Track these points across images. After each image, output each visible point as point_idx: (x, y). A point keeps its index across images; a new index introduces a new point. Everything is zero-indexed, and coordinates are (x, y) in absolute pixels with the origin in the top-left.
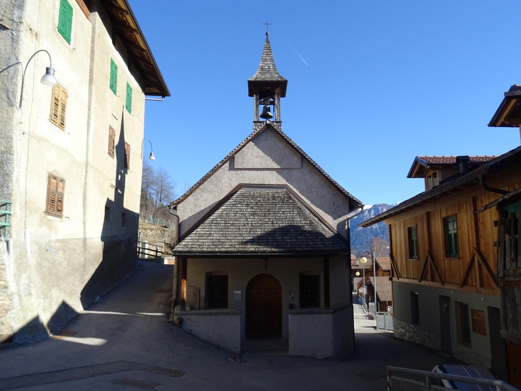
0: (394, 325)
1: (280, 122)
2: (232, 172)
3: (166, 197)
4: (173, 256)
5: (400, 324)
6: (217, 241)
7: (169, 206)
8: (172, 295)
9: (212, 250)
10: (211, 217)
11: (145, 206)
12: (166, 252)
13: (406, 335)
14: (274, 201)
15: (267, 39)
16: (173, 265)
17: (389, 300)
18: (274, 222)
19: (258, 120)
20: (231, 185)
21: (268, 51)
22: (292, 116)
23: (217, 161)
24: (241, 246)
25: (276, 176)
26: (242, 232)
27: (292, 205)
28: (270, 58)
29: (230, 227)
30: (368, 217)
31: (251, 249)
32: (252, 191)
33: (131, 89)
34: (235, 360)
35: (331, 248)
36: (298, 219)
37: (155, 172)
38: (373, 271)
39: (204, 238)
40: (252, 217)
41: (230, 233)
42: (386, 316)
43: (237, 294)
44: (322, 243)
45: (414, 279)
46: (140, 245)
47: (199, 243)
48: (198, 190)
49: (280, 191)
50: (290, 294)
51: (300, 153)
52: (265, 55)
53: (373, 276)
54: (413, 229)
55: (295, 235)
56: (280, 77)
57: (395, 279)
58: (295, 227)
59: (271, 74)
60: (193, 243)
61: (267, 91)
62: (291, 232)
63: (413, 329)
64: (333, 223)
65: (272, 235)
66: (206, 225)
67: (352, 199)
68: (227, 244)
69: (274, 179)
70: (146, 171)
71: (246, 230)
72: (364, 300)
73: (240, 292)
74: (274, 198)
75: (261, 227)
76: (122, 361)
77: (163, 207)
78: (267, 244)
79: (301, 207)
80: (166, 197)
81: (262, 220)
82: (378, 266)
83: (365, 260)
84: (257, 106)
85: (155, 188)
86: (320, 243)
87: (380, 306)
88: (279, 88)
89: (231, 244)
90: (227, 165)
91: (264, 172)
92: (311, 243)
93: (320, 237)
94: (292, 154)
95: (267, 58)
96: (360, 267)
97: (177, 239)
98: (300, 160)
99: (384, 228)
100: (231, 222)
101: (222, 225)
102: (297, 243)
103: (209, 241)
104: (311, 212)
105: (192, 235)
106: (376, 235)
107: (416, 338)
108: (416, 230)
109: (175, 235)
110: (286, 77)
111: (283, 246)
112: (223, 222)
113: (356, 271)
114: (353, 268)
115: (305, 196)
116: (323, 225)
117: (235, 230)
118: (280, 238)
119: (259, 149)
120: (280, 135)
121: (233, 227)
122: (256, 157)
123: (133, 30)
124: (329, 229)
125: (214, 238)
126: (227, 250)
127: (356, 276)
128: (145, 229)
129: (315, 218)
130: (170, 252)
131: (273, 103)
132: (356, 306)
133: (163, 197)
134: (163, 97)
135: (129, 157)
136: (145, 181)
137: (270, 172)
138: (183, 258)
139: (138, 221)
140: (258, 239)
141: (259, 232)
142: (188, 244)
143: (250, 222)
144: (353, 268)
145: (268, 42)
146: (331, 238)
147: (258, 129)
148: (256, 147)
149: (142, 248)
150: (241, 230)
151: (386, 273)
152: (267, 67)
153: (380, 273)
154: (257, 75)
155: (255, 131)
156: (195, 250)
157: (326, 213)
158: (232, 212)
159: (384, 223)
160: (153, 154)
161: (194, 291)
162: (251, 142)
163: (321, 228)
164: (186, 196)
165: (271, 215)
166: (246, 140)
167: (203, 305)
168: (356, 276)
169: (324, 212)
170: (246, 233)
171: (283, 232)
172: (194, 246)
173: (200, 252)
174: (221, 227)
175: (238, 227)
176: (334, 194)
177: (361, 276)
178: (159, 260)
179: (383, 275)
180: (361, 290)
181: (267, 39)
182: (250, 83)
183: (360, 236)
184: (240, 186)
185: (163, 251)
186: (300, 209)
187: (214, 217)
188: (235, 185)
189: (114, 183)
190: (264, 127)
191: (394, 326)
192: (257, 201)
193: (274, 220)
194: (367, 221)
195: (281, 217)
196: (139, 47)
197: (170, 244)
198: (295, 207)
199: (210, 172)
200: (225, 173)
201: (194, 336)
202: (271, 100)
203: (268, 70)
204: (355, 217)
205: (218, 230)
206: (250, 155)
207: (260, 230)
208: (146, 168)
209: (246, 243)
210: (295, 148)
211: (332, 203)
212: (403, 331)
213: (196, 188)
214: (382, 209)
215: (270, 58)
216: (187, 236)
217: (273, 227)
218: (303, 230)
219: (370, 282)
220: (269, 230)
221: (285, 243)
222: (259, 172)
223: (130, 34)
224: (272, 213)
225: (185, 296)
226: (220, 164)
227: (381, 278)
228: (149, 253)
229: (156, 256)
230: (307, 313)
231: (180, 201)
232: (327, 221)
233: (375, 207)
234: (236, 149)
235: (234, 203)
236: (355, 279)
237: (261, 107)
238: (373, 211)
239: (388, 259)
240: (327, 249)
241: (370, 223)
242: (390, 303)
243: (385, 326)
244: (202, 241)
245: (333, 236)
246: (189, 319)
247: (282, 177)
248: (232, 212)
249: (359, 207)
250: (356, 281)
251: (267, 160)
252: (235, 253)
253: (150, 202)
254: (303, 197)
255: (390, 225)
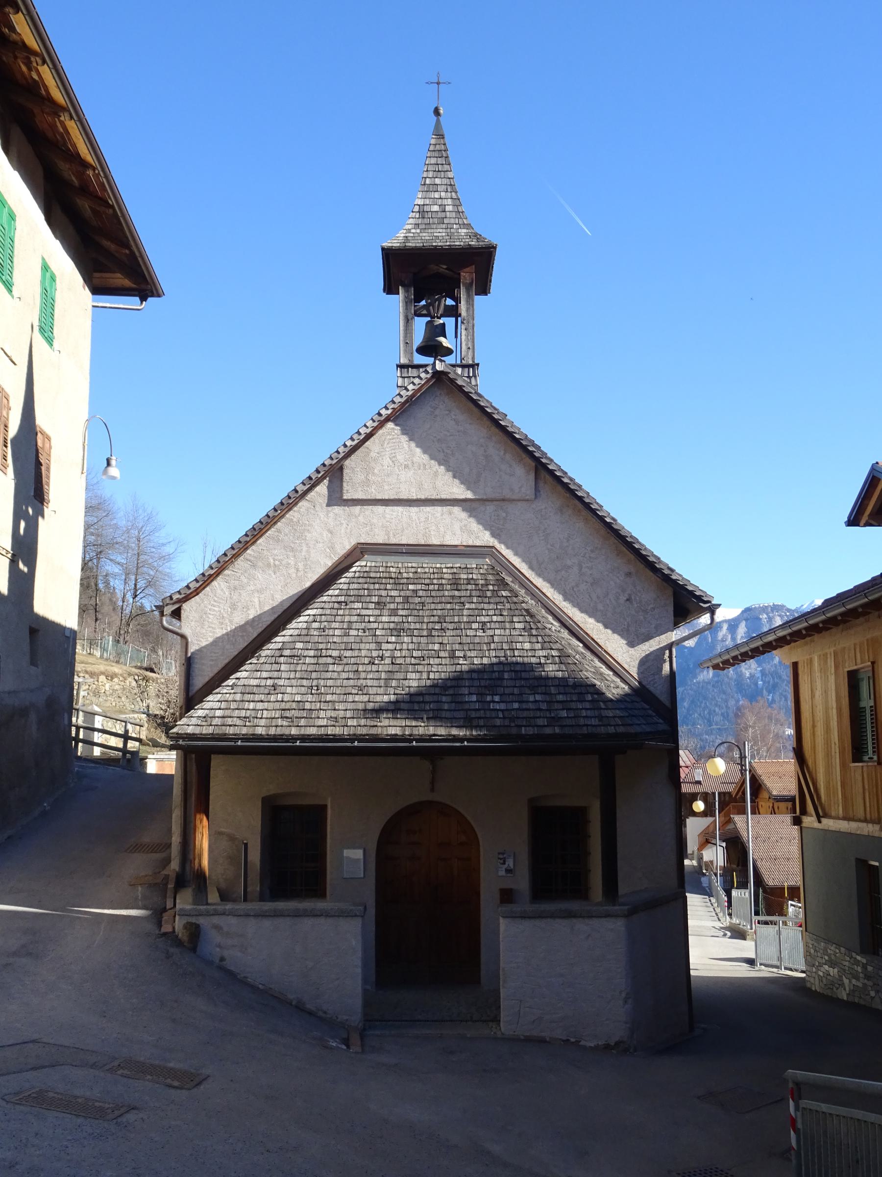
0: (807, 955)
1: (474, 366)
2: (337, 509)
3: (149, 584)
4: (171, 748)
5: (825, 952)
6: (294, 705)
7: (161, 609)
8: (167, 861)
9: (279, 731)
10: (278, 639)
11: (92, 612)
12: (152, 740)
13: (842, 985)
14: (457, 593)
15: (438, 125)
16: (172, 775)
17: (792, 883)
18: (458, 654)
19: (411, 360)
20: (332, 548)
21: (440, 161)
22: (503, 345)
23: (295, 479)
24: (363, 722)
25: (461, 521)
26: (364, 682)
27: (508, 606)
28: (445, 181)
29: (331, 668)
30: (729, 643)
31: (392, 731)
32: (395, 564)
33: (53, 279)
34: (348, 1046)
35: (621, 730)
36: (527, 646)
37: (121, 514)
38: (744, 800)
39: (257, 698)
40: (393, 639)
41: (330, 683)
42: (785, 932)
43: (350, 858)
44: (596, 713)
45: (865, 821)
46: (79, 719)
47: (243, 713)
48: (240, 562)
49: (473, 563)
50: (503, 859)
51: (531, 454)
52: (431, 174)
53: (743, 811)
54: (864, 676)
55: (516, 691)
56: (476, 235)
57: (809, 821)
58: (518, 668)
59: (449, 227)
60: (228, 713)
61: (436, 276)
62: (505, 683)
63: (864, 967)
64: (628, 656)
65: (451, 692)
66: (262, 660)
67: (683, 587)
68: (322, 714)
69: (458, 529)
70: (95, 508)
71: (376, 675)
72: (718, 884)
73: (358, 854)
74: (455, 583)
75: (420, 668)
76: (34, 1041)
77: (141, 612)
78: (436, 717)
79: (533, 610)
80: (149, 584)
81: (423, 646)
82: (757, 786)
83: (719, 765)
84: (408, 321)
85: (120, 559)
86: (589, 713)
87: (765, 898)
88: (472, 268)
89: (335, 714)
90: (322, 489)
91: (428, 509)
92: (564, 714)
93: (589, 697)
94: (508, 456)
95: (438, 181)
96: (706, 788)
97: (180, 701)
98: (532, 476)
99: (775, 674)
100: (335, 653)
101: (308, 660)
102: (525, 714)
103: (270, 706)
104: (564, 625)
105: (224, 690)
106: (753, 696)
107: (873, 994)
108: (874, 677)
109: (175, 692)
110: (490, 236)
111: (481, 723)
112: (312, 653)
113: (694, 797)
114: (685, 788)
115: (546, 579)
116: (596, 661)
117: (344, 675)
118: (474, 698)
119: (413, 444)
120: (475, 403)
121: (340, 668)
122: (406, 466)
123: (57, 109)
124: (616, 673)
125: (287, 698)
126: (322, 731)
127: (695, 814)
128: (92, 674)
129: (575, 642)
130: (163, 739)
131: (453, 312)
132: (694, 901)
133: (141, 584)
134: (143, 299)
135: (48, 469)
136: (92, 538)
137: (446, 509)
138: (198, 755)
139: (74, 653)
140: (410, 702)
141: (414, 682)
142: (211, 716)
143: (387, 654)
144: (685, 788)
145: (440, 135)
146: (623, 700)
147: (411, 387)
148: (404, 438)
149: (85, 728)
150: (363, 675)
151: (782, 805)
152: (436, 208)
153: (764, 804)
154: (409, 231)
155: (403, 393)
156: (231, 731)
157: (606, 627)
158: (337, 625)
159: (778, 659)
160: (113, 462)
161: (231, 847)
162: (390, 425)
163: (592, 671)
164: (206, 580)
165: (449, 633)
166: (376, 418)
167: (255, 887)
168: (695, 814)
169: (600, 626)
170: (375, 683)
171: (483, 683)
172: (229, 721)
173: (246, 738)
174: (304, 668)
175: (355, 668)
176: (629, 574)
177: (708, 812)
178: (131, 762)
179: (773, 812)
180: (708, 855)
181: (438, 125)
182: (389, 254)
183: (705, 698)
184: (360, 551)
185: (143, 737)
186: (532, 616)
187: (286, 639)
188: (344, 546)
189: (8, 545)
190: (428, 380)
191: (805, 957)
192: (408, 593)
193: (457, 647)
194: (728, 651)
195: (477, 640)
196: (75, 158)
197: (163, 718)
198: (517, 608)
199: (275, 510)
200: (315, 510)
201: (231, 974)
202: (450, 302)
203: (440, 215)
204: (690, 643)
205: (298, 675)
206: (387, 461)
207: (418, 676)
208: (94, 502)
209: (377, 712)
210: (517, 442)
211: (623, 598)
212: (834, 972)
213: (236, 556)
214: (770, 619)
215: (445, 181)
216: (210, 693)
217: (453, 668)
218: (541, 678)
219: (736, 830)
220: (443, 676)
221: (488, 714)
222: (414, 510)
223: (50, 119)
224: (451, 626)
225: (205, 862)
226: (301, 489)
227: (765, 819)
228: (104, 743)
229: (124, 750)
230: (553, 916)
231: (190, 593)
232: (610, 650)
233: (750, 615)
234: (349, 443)
235: (342, 599)
236: (690, 822)
237: (420, 324)
238: (743, 625)
239: (789, 763)
240: (611, 730)
241: (735, 658)
242: (794, 893)
243: (780, 959)
244: (252, 706)
245: (626, 695)
246: (218, 928)
247: (479, 523)
248: (337, 625)
249: (703, 611)
250: (694, 827)
251: (436, 474)
252: (345, 740)
253: (106, 599)
254: (539, 582)
255: (795, 665)
